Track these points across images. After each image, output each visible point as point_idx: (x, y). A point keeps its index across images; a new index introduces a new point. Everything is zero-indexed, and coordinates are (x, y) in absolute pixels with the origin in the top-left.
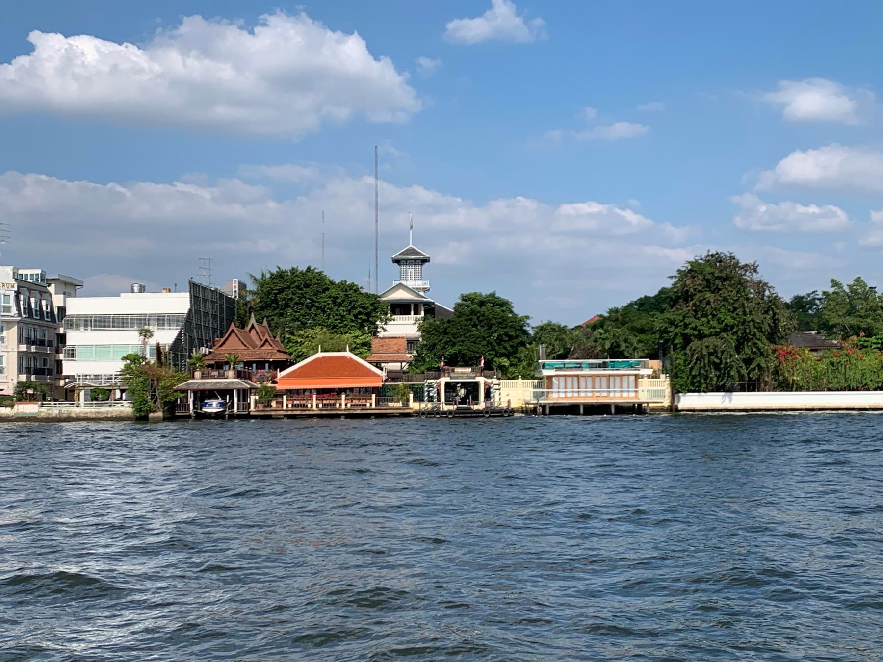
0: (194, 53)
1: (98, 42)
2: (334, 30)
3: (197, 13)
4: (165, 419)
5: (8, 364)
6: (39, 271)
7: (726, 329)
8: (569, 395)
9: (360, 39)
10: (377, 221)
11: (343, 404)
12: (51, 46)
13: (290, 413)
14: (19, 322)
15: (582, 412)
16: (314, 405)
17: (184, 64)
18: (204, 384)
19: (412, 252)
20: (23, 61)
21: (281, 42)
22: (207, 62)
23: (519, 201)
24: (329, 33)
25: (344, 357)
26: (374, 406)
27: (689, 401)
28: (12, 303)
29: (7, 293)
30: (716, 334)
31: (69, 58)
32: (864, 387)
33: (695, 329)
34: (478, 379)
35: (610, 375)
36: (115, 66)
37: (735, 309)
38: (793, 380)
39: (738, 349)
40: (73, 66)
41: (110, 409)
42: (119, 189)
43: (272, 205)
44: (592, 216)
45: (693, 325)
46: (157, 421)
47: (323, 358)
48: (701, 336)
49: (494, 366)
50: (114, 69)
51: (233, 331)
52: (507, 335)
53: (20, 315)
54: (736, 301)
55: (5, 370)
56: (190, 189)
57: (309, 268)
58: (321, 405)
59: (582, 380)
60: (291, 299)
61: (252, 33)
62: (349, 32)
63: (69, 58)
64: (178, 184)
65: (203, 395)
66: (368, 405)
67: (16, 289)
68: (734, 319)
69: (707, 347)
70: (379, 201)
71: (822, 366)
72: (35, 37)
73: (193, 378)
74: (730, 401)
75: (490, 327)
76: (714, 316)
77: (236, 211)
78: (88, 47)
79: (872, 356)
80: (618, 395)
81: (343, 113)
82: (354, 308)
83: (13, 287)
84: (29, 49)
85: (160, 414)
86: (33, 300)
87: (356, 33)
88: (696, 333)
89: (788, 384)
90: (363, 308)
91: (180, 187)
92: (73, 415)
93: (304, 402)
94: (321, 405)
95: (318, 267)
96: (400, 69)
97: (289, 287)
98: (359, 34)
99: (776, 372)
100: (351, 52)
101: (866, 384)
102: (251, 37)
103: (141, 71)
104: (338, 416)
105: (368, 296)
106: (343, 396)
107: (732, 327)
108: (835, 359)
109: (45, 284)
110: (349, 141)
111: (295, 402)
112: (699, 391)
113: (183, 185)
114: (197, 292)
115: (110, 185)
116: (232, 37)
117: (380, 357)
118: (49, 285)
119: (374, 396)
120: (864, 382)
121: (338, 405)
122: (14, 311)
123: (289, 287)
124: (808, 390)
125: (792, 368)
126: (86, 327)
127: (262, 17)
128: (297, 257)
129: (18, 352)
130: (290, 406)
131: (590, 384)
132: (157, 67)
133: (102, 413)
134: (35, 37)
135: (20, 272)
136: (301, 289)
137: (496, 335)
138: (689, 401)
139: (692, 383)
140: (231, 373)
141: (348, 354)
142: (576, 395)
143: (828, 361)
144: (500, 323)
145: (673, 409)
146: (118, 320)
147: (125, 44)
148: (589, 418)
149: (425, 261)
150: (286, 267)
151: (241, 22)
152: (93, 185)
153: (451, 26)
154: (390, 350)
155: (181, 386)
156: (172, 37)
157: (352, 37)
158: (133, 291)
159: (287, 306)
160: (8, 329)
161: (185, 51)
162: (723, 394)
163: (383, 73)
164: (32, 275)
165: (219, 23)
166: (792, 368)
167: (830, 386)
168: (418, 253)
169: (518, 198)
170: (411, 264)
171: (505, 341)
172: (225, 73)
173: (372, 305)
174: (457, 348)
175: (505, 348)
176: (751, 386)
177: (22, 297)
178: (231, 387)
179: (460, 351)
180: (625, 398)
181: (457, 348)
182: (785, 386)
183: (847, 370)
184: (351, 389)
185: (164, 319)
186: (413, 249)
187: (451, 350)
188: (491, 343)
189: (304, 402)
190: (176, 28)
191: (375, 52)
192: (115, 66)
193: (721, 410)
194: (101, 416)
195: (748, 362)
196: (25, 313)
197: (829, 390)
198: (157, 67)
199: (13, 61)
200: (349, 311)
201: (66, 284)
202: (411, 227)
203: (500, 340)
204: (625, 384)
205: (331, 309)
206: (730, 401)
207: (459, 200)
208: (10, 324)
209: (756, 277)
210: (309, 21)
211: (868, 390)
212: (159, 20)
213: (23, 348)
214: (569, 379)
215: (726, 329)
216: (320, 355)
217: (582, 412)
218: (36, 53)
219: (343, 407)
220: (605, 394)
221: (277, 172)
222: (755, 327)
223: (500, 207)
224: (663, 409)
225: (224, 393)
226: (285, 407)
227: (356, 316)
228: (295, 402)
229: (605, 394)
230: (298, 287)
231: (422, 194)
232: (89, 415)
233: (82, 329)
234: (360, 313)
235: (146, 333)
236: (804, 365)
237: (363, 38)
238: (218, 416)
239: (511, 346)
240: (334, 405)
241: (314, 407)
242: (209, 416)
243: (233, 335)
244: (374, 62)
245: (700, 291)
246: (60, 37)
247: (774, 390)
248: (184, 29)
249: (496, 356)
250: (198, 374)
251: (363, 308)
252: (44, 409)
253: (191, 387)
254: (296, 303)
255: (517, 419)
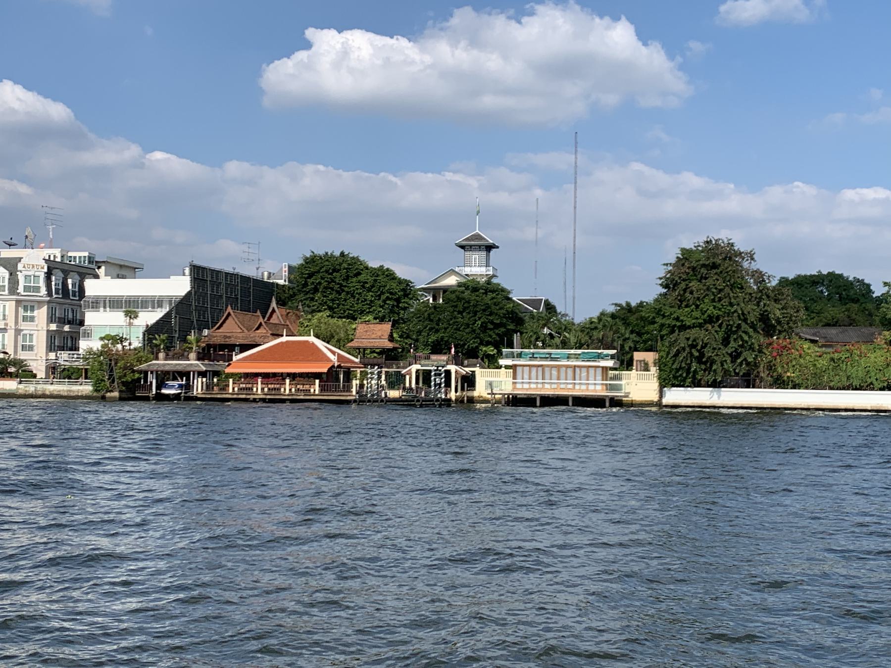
0: (463, 44)
1: (371, 35)
2: (601, 17)
3: (467, 5)
4: (121, 399)
5: (37, 342)
6: (86, 254)
7: (711, 320)
8: (533, 386)
9: (628, 24)
10: (575, 208)
11: (287, 388)
12: (327, 41)
13: (235, 396)
14: (49, 302)
15: (538, 404)
16: (259, 389)
17: (453, 55)
18: (164, 365)
19: (477, 237)
20: (302, 55)
21: (549, 32)
22: (475, 52)
23: (798, 187)
24: (597, 20)
25: (307, 342)
26: (317, 392)
27: (677, 396)
28: (42, 284)
29: (37, 274)
30: (700, 326)
31: (345, 53)
32: (870, 387)
33: (677, 319)
34: (449, 367)
35: (575, 366)
36: (388, 59)
37: (720, 300)
38: (788, 377)
39: (726, 342)
40: (346, 61)
41: (81, 388)
42: (394, 179)
43: (538, 192)
44: (876, 202)
45: (675, 315)
46: (113, 400)
47: (287, 342)
48: (683, 328)
49: (481, 354)
50: (387, 60)
51: (229, 314)
52: (492, 323)
53: (50, 294)
54: (720, 291)
55: (35, 348)
56: (459, 177)
57: (342, 254)
58: (266, 389)
59: (519, 369)
60: (320, 283)
61: (519, 22)
62: (616, 19)
63: (345, 53)
64: (447, 173)
65: (163, 377)
66: (312, 390)
67: (46, 270)
68: (720, 309)
69: (688, 339)
70: (573, 186)
71: (823, 363)
72: (311, 33)
73: (157, 358)
74: (719, 397)
75: (475, 313)
76: (697, 306)
77: (502, 199)
78: (361, 43)
79: (879, 353)
80: (526, 386)
81: (611, 99)
82: (382, 293)
83: (43, 268)
84: (307, 45)
85: (116, 394)
86: (70, 281)
87: (623, 18)
88: (678, 324)
89: (784, 381)
90: (391, 293)
91: (449, 176)
92: (48, 393)
93: (250, 386)
94: (266, 389)
95: (353, 252)
96: (671, 56)
97: (318, 272)
98: (628, 19)
99: (770, 367)
100: (619, 38)
101: (871, 383)
102: (518, 25)
103: (413, 62)
104: (283, 401)
105: (400, 282)
106: (288, 381)
107: (718, 318)
108: (836, 356)
109: (93, 266)
110: (613, 126)
111: (241, 386)
112: (683, 386)
113: (451, 174)
114: (199, 274)
115: (382, 174)
116: (500, 26)
117: (361, 342)
118: (99, 268)
119: (317, 381)
120: (869, 381)
121: (282, 390)
122: (43, 291)
123: (318, 272)
124: (807, 388)
125: (787, 364)
126: (105, 307)
127: (528, 6)
128: (330, 242)
129: (48, 331)
130: (236, 389)
131: (584, 374)
132: (428, 59)
133: (74, 391)
134: (311, 33)
135: (70, 254)
136: (331, 274)
137: (479, 322)
138: (677, 396)
139: (675, 377)
140: (193, 355)
141: (312, 339)
142: (540, 386)
143: (829, 356)
144: (484, 310)
145: (659, 404)
146: (146, 301)
147: (395, 37)
148: (546, 409)
149: (489, 248)
150: (320, 252)
151: (512, 12)
152: (367, 174)
153: (723, 8)
154: (373, 336)
155: (143, 366)
156: (441, 29)
157: (620, 22)
158: (184, 275)
159: (316, 290)
160: (39, 308)
161: (454, 44)
162: (711, 389)
163: (653, 59)
164: (80, 257)
165: (490, 14)
166: (787, 364)
167: (832, 384)
168: (482, 238)
169: (796, 183)
170: (475, 250)
171: (491, 329)
172: (492, 62)
173: (403, 290)
174: (440, 335)
175: (490, 336)
176: (748, 381)
177: (53, 278)
178: (188, 369)
179: (442, 338)
180: (583, 391)
181: (440, 335)
182: (780, 383)
183: (849, 366)
184: (236, 374)
185: (105, 301)
186: (479, 235)
187: (433, 338)
188: (474, 331)
189: (250, 386)
190: (447, 20)
191: (644, 37)
192: (388, 59)
193: (709, 407)
194: (72, 394)
195: (735, 356)
196: (57, 293)
197: (831, 388)
198: (428, 59)
199: (292, 57)
200: (379, 296)
201: (121, 266)
202: (478, 212)
203: (484, 328)
204: (563, 375)
205: (360, 294)
206: (719, 397)
207: (732, 186)
208: (40, 303)
209: (754, 266)
210: (577, 8)
211: (873, 389)
212: (431, 14)
213: (53, 327)
214: (534, 370)
215: (711, 320)
216: (284, 339)
217: (538, 404)
218: (313, 49)
219: (287, 392)
220: (570, 386)
221: (541, 160)
222: (740, 319)
223: (776, 194)
224: (650, 404)
225: (184, 374)
226: (231, 391)
227: (384, 301)
228: (241, 386)
229: (570, 386)
230: (327, 271)
231: (693, 180)
232: (62, 393)
233: (102, 309)
234: (388, 298)
235: (131, 314)
236: (802, 361)
237: (632, 23)
238: (177, 397)
239: (498, 335)
240: (279, 389)
241: (259, 391)
242: (167, 398)
243: (230, 318)
244: (643, 48)
245: (684, 280)
246: (333, 33)
247: (771, 386)
248: (455, 21)
249: (481, 343)
250: (161, 355)
251: (391, 293)
252: (21, 386)
253: (151, 368)
254: (325, 288)
255: (480, 412)
